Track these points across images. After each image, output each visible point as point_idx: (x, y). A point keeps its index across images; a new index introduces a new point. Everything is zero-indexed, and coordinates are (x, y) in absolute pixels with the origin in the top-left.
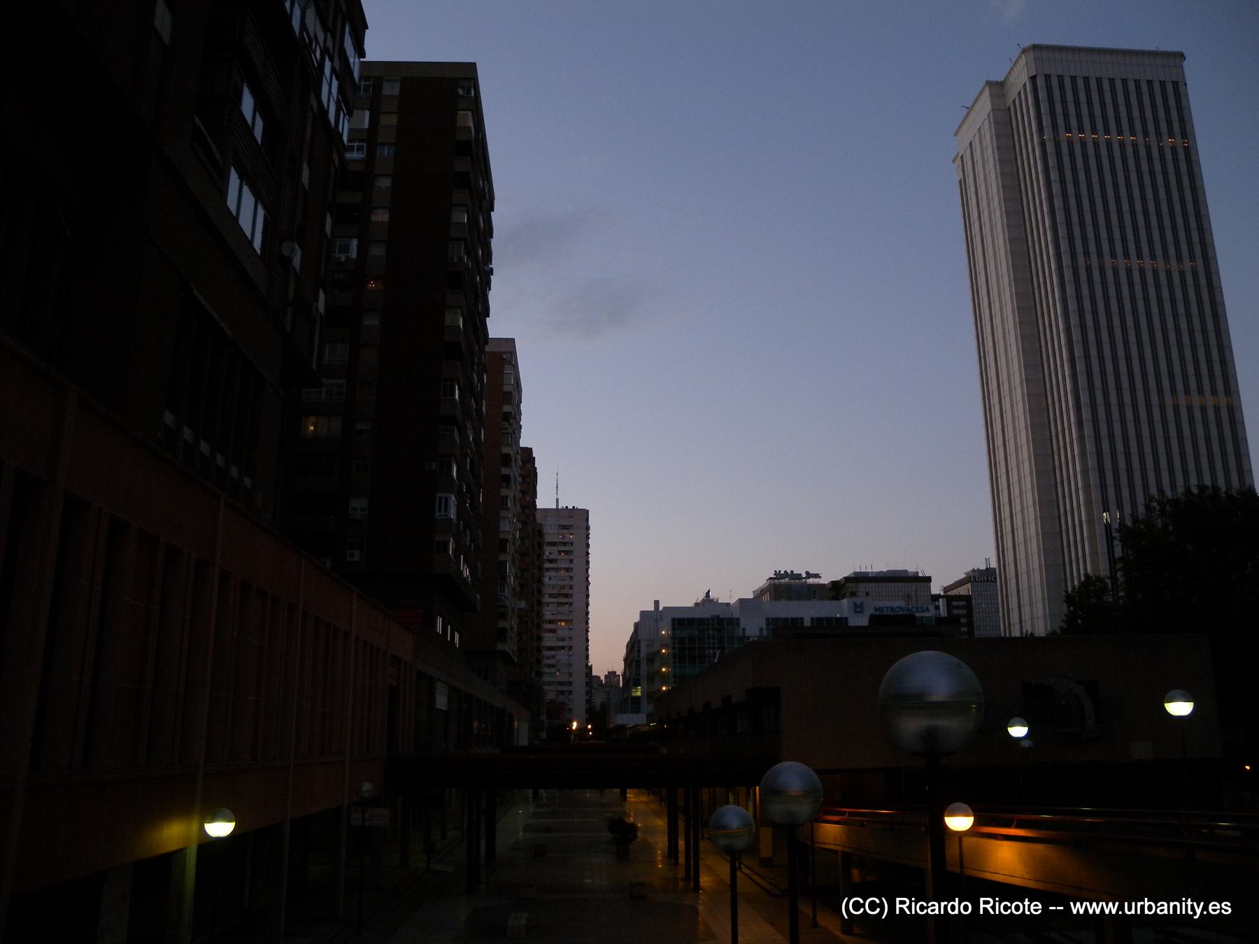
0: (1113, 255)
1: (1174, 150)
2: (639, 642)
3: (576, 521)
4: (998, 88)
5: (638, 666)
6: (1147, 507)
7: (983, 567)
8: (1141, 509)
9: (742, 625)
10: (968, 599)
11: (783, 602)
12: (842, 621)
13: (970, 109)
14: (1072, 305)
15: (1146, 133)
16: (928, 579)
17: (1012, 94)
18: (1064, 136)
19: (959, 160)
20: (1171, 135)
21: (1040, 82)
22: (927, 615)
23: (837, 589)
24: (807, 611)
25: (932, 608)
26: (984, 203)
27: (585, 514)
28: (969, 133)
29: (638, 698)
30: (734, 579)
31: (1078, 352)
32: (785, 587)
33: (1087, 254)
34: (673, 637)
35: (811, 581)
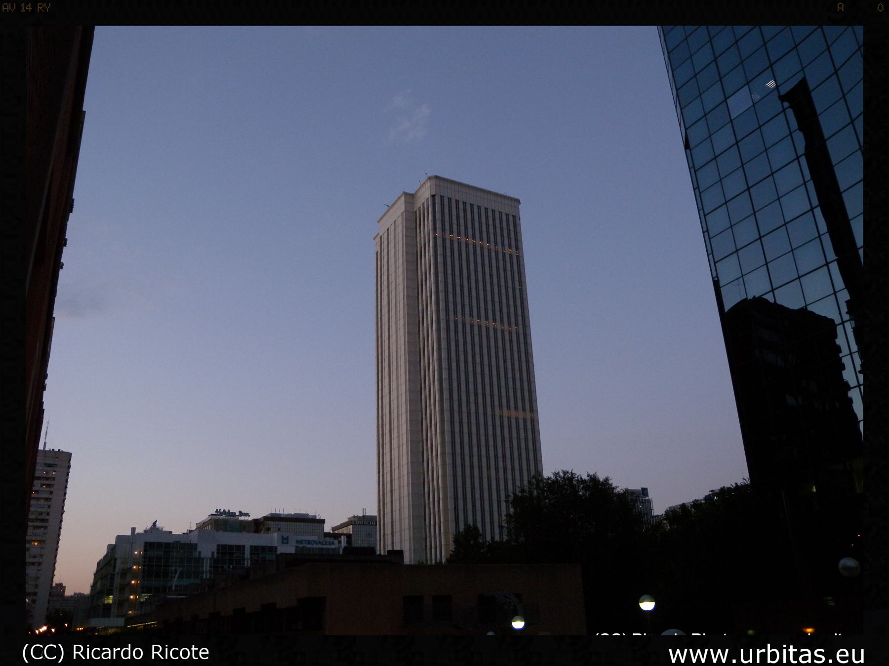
0: (471, 316)
1: (511, 256)
2: (116, 560)
3: (62, 460)
4: (410, 198)
5: (112, 579)
6: (529, 482)
7: (361, 515)
8: (526, 483)
9: (199, 549)
10: (349, 536)
11: (221, 533)
12: (272, 549)
13: (390, 208)
14: (444, 344)
15: (496, 243)
16: (323, 521)
17: (419, 203)
18: (448, 235)
19: (378, 239)
20: (510, 247)
21: (437, 200)
22: (333, 547)
23: (258, 525)
24: (249, 540)
25: (336, 542)
26: (392, 270)
27: (69, 455)
28: (388, 222)
29: (109, 605)
30: (181, 515)
31: (445, 375)
32: (223, 522)
33: (455, 313)
34: (145, 557)
35: (242, 518)
